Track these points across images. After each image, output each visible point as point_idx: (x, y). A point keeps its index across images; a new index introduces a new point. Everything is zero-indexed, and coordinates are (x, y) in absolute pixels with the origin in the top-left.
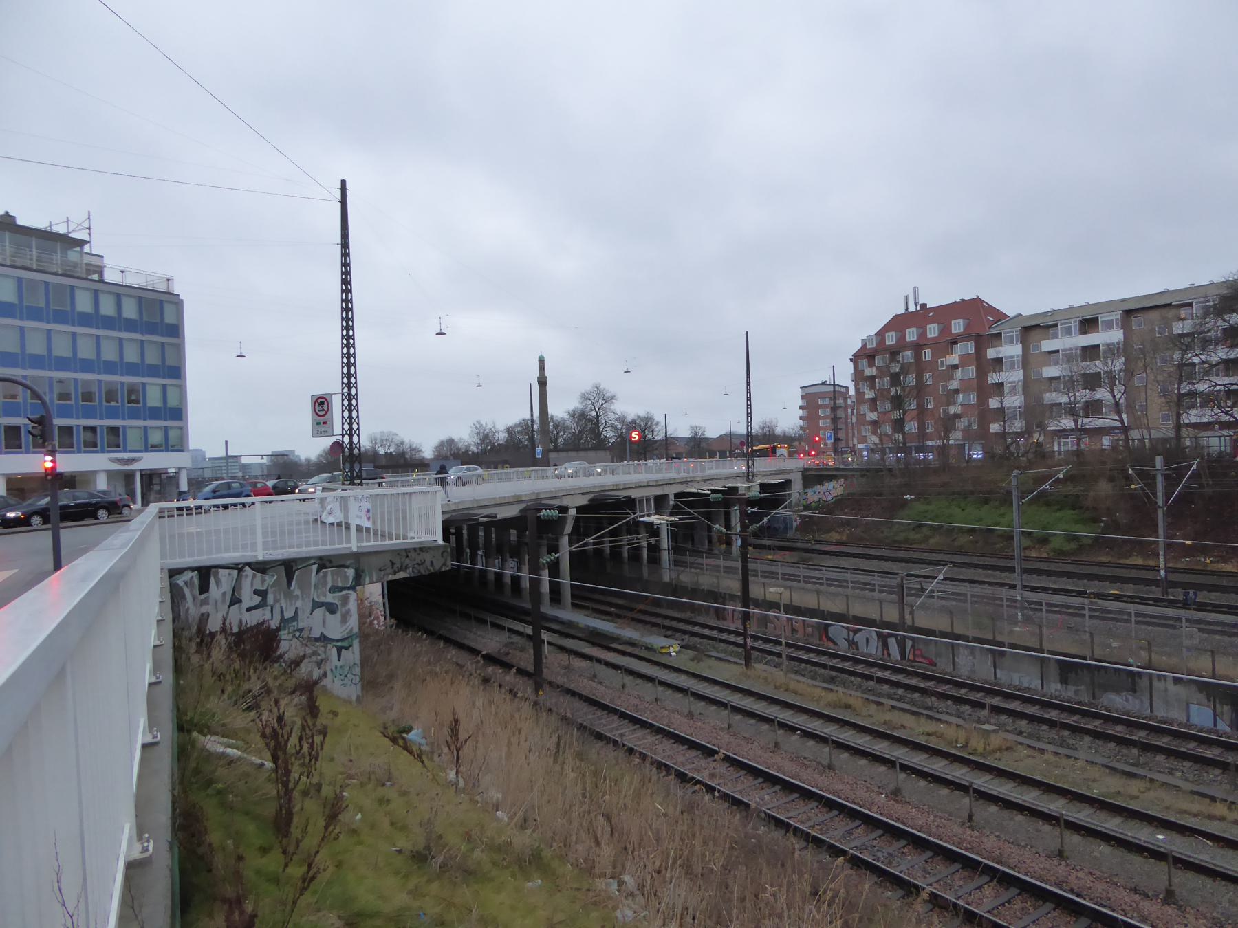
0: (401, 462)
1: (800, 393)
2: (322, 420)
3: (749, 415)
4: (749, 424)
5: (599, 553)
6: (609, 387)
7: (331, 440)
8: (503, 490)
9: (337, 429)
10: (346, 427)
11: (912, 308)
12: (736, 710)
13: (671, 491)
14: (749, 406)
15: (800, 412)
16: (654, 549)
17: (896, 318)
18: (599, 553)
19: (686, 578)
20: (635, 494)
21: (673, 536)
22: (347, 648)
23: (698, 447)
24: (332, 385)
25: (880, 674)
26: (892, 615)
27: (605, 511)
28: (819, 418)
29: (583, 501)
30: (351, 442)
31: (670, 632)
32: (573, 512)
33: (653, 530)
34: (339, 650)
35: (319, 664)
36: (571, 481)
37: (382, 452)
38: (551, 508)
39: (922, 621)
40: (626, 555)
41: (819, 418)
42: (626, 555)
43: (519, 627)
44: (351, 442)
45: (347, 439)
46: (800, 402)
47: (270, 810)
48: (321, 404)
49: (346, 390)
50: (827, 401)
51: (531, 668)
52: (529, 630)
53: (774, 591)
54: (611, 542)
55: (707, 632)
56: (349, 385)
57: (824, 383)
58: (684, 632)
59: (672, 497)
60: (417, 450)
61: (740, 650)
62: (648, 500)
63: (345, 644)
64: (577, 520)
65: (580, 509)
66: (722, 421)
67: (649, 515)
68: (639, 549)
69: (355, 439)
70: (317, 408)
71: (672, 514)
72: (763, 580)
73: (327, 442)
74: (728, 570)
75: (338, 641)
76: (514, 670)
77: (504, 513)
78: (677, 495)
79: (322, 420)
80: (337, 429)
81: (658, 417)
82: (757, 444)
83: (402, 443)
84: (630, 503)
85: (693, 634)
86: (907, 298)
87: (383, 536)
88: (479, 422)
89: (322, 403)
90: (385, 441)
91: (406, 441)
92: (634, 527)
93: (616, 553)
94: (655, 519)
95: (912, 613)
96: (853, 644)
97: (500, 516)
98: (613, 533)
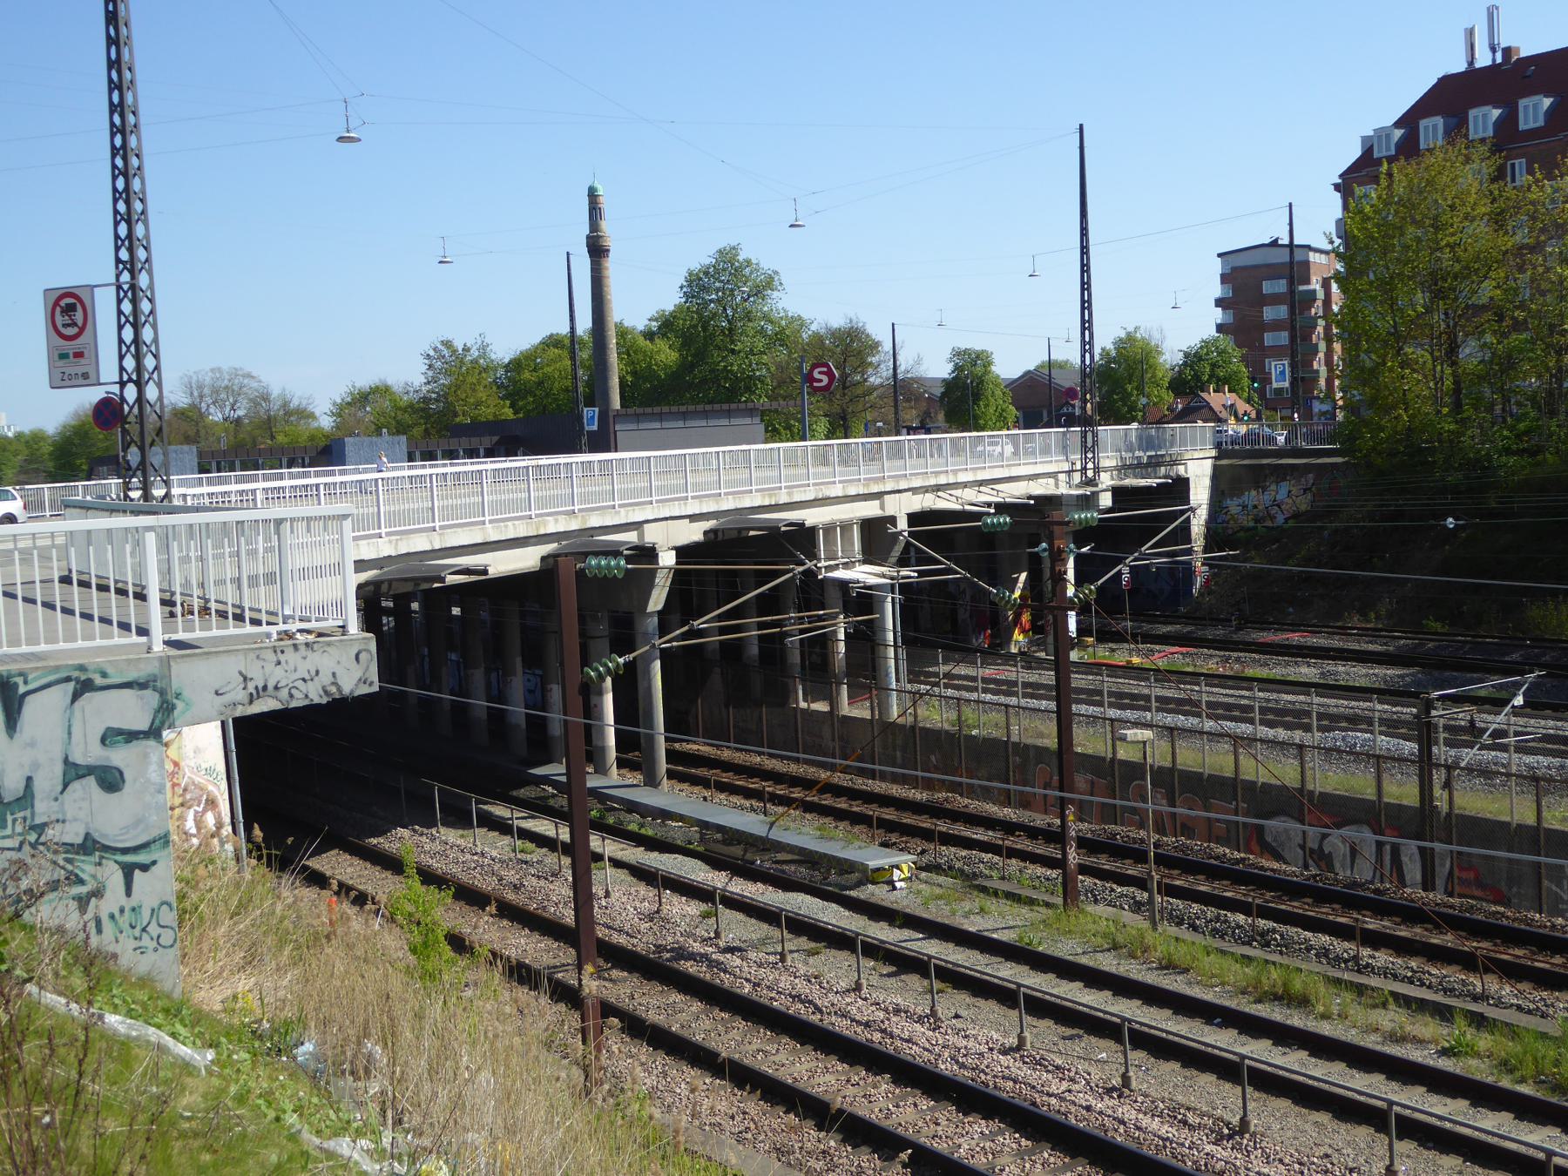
0: (263, 441)
1: (1217, 267)
2: (70, 347)
3: (1086, 325)
4: (1087, 345)
5: (732, 651)
6: (760, 252)
7: (94, 395)
8: (498, 517)
9: (108, 369)
10: (130, 363)
11: (1483, 59)
12: (1040, 1007)
13: (900, 508)
14: (1086, 304)
15: (1218, 315)
16: (865, 639)
17: (1446, 83)
18: (732, 651)
19: (935, 716)
20: (811, 517)
21: (908, 615)
22: (145, 868)
23: (962, 401)
24: (91, 265)
25: (1372, 924)
26: (1402, 790)
27: (749, 558)
28: (1265, 327)
29: (693, 533)
30: (140, 399)
31: (893, 833)
32: (667, 559)
33: (861, 601)
34: (128, 871)
35: (83, 902)
36: (660, 495)
37: (216, 416)
38: (613, 552)
39: (1474, 801)
40: (795, 657)
41: (1265, 327)
42: (795, 657)
43: (544, 826)
44: (140, 399)
45: (131, 393)
46: (1217, 290)
47: (200, 349)
48: (68, 310)
49: (126, 277)
50: (1281, 286)
51: (568, 917)
52: (565, 835)
53: (1139, 740)
54: (761, 626)
55: (980, 834)
56: (132, 267)
57: (1274, 243)
58: (927, 835)
59: (902, 524)
60: (304, 414)
61: (1053, 873)
62: (846, 527)
63: (141, 858)
64: (679, 576)
65: (683, 552)
66: (1028, 335)
67: (846, 566)
68: (826, 641)
69: (151, 393)
70: (59, 320)
71: (903, 562)
72: (1113, 713)
73: (88, 397)
74: (1033, 690)
75: (125, 851)
76: (492, 908)
77: (502, 564)
78: (914, 519)
79: (70, 347)
80: (108, 369)
81: (878, 331)
82: (1110, 388)
83: (266, 397)
84: (804, 538)
85: (947, 839)
86: (1470, 33)
87: (222, 615)
88: (448, 344)
89: (70, 309)
90: (226, 390)
91: (275, 392)
92: (813, 592)
93: (773, 647)
94: (865, 574)
95: (1447, 785)
96: (1322, 858)
97: (494, 572)
98: (769, 604)
